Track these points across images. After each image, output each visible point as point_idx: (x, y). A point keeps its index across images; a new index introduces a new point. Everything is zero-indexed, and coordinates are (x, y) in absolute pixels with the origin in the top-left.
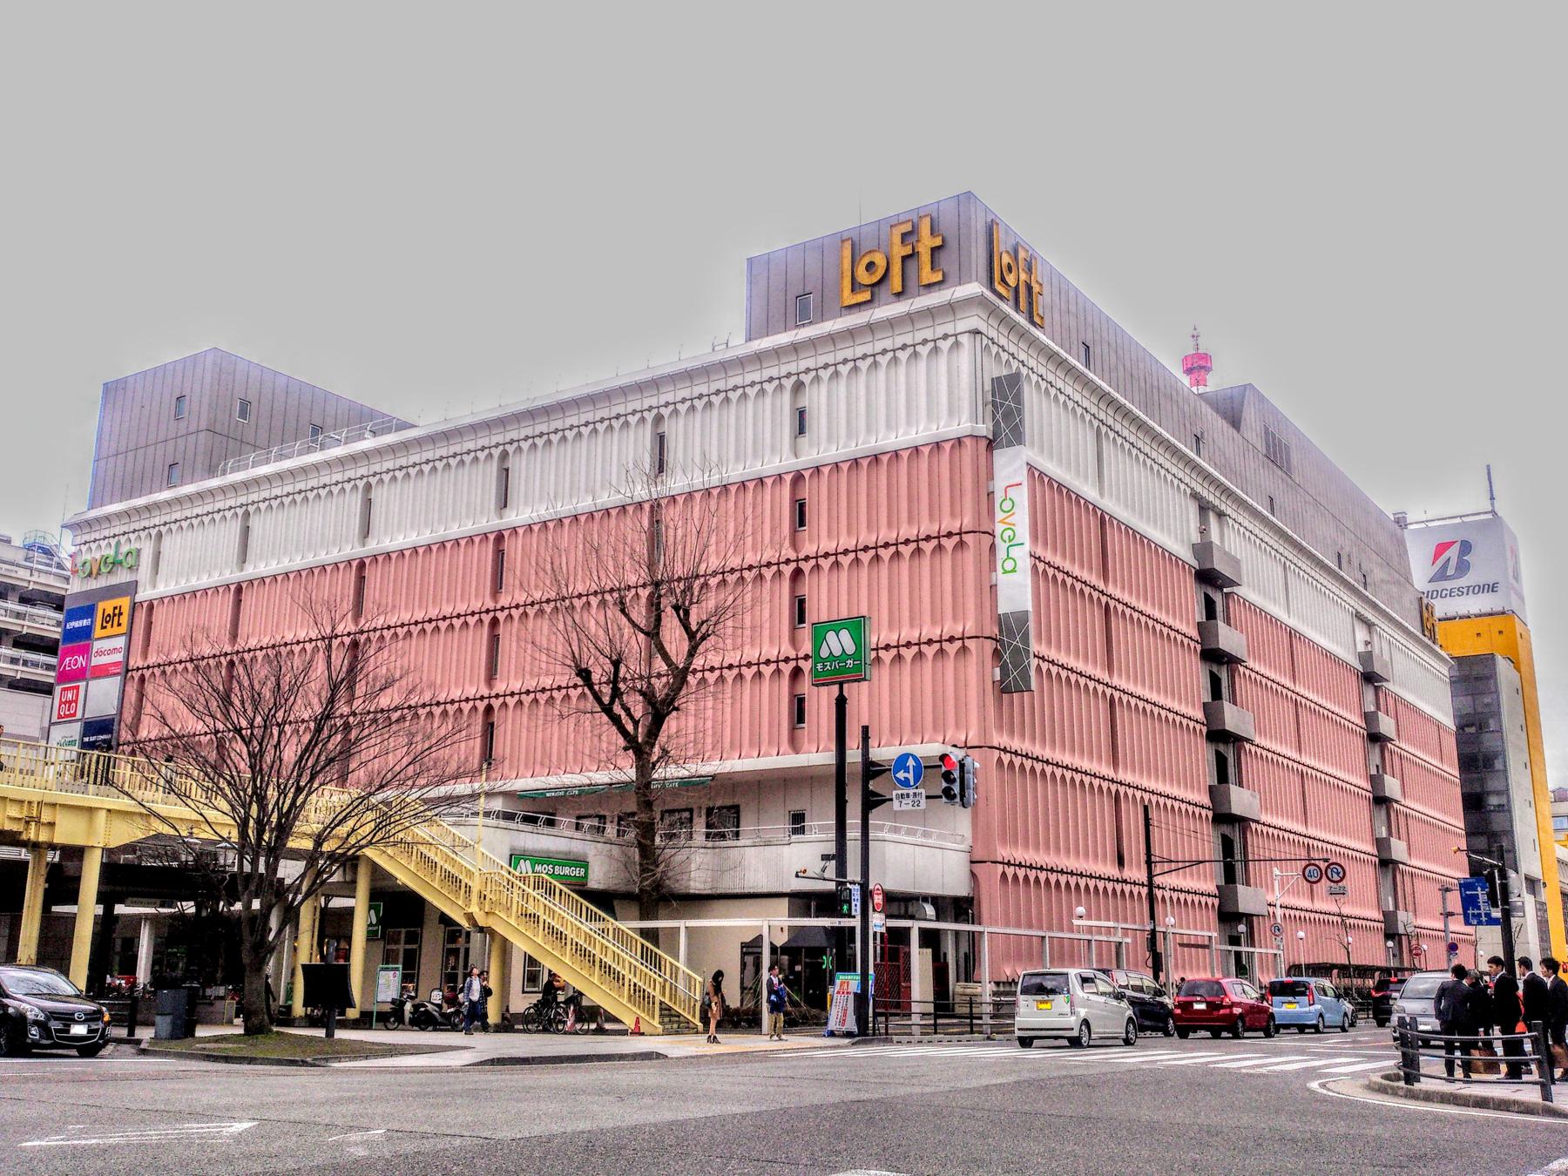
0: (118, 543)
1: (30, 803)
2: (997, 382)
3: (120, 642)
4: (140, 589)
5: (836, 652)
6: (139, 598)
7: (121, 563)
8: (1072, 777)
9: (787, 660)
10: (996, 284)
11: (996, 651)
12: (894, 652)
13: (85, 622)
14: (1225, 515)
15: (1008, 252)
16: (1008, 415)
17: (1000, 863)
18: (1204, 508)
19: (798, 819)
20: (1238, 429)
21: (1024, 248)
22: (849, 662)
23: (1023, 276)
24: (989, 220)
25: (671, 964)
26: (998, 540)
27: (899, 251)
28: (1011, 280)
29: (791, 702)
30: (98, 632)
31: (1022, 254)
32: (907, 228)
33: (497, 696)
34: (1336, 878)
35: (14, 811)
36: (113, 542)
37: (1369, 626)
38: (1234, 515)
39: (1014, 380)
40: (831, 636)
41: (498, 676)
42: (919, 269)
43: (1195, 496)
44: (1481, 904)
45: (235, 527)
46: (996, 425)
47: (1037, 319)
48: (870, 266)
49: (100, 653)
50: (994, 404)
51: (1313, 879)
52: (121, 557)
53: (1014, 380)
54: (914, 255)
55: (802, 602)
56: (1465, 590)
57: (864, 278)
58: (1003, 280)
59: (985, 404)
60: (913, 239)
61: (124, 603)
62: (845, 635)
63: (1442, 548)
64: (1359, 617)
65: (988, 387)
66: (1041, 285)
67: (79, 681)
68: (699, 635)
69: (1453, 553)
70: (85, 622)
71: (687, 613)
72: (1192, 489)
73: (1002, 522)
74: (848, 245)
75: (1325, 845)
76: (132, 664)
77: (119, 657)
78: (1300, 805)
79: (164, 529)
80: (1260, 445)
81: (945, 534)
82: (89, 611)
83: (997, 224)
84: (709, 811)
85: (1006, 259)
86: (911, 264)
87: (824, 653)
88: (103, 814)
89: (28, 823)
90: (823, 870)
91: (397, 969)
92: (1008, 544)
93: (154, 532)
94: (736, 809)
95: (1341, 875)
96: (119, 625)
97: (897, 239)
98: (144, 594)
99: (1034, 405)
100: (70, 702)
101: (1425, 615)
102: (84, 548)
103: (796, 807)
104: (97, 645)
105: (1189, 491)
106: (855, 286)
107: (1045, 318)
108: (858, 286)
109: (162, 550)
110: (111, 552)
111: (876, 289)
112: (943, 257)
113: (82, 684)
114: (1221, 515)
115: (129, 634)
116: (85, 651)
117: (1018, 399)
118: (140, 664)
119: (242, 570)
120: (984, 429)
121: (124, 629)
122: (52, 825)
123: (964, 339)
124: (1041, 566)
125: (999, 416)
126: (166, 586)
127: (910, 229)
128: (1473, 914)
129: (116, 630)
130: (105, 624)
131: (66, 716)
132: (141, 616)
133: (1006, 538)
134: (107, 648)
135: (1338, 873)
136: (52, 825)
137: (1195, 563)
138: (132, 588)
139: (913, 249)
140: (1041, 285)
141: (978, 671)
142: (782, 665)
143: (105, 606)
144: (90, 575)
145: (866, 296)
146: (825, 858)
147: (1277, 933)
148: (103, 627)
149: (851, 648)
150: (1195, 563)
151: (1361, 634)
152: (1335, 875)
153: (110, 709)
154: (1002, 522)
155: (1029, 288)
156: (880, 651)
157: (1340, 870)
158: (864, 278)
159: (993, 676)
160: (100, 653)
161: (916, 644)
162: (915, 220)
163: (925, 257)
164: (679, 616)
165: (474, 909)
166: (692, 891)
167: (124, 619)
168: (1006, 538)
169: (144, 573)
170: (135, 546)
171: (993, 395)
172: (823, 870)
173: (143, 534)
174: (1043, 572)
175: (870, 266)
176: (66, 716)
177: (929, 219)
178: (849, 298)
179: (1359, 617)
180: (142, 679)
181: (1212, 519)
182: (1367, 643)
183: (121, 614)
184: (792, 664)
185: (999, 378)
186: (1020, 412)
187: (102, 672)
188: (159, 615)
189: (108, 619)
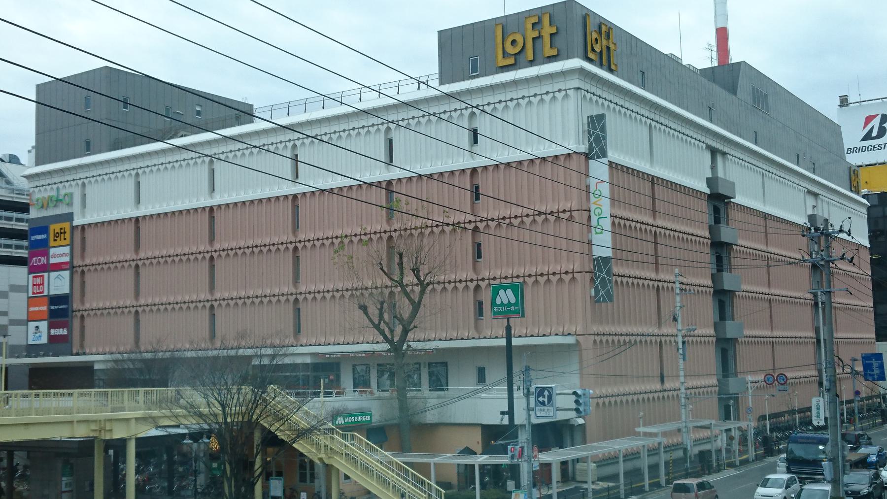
0: (58, 188)
1: (100, 421)
2: (591, 119)
3: (67, 250)
4: (75, 218)
5: (506, 302)
6: (75, 223)
7: (61, 201)
8: (635, 117)
9: (472, 280)
10: (589, 53)
11: (592, 279)
12: (533, 278)
13: (43, 237)
14: (726, 154)
15: (595, 31)
16: (598, 140)
17: (593, 335)
18: (714, 152)
19: (481, 376)
20: (734, 92)
21: (604, 24)
22: (512, 307)
23: (605, 42)
24: (584, 13)
25: (428, 484)
26: (592, 214)
27: (531, 34)
28: (597, 48)
29: (475, 304)
30: (52, 243)
31: (604, 29)
32: (535, 20)
33: (301, 293)
34: (782, 382)
35: (93, 427)
36: (55, 187)
37: (816, 195)
38: (732, 152)
39: (601, 117)
40: (501, 292)
41: (300, 281)
42: (543, 47)
43: (708, 147)
44: (874, 369)
45: (131, 183)
46: (591, 145)
47: (613, 67)
48: (514, 42)
49: (55, 256)
50: (589, 132)
51: (770, 383)
52: (61, 198)
53: (601, 117)
54: (540, 37)
55: (479, 246)
56: (883, 146)
57: (510, 50)
58: (593, 50)
59: (584, 132)
60: (538, 27)
61: (66, 226)
62: (509, 291)
63: (869, 119)
64: (810, 192)
65: (586, 121)
66: (615, 44)
67: (44, 272)
68: (425, 282)
69: (876, 122)
70: (43, 237)
71: (418, 272)
72: (707, 144)
73: (594, 203)
74: (499, 29)
75: (783, 340)
76: (75, 263)
77: (67, 259)
78: (768, 320)
79: (86, 181)
80: (750, 100)
81: (562, 211)
82: (44, 230)
83: (589, 15)
84: (430, 364)
85: (595, 35)
86: (538, 42)
87: (498, 302)
88: (133, 421)
89: (100, 431)
90: (502, 420)
91: (281, 479)
92: (598, 217)
93: (80, 182)
94: (445, 364)
95: (785, 380)
96: (65, 239)
97: (529, 26)
98: (77, 222)
99: (614, 125)
100: (39, 285)
101: (853, 177)
102: (36, 190)
103: (481, 365)
104: (52, 251)
105: (704, 146)
106: (505, 54)
107: (618, 65)
108: (506, 55)
109: (86, 193)
110: (54, 193)
111: (518, 57)
112: (558, 40)
113: (46, 275)
114: (724, 154)
115: (72, 245)
116: (46, 254)
117: (603, 130)
118: (81, 263)
119: (138, 208)
120: (583, 148)
121: (68, 242)
122: (111, 430)
123: (570, 92)
124: (617, 221)
125: (592, 140)
126: (91, 217)
127: (537, 21)
128: (870, 375)
129: (63, 242)
130: (56, 238)
131: (38, 293)
132: (78, 235)
133: (597, 214)
134: (59, 253)
135: (783, 380)
136: (111, 430)
137: (708, 191)
138: (69, 217)
139: (539, 33)
140: (615, 44)
141: (583, 290)
142: (469, 283)
143: (55, 227)
144: (42, 207)
145: (511, 61)
146: (503, 413)
147: (749, 412)
148: (55, 240)
149: (513, 300)
150: (708, 191)
151: (811, 201)
152: (782, 380)
153: (66, 290)
154: (594, 203)
155: (608, 48)
156: (526, 278)
157: (784, 377)
158: (510, 50)
159: (590, 292)
160: (55, 256)
161: (546, 275)
162: (540, 15)
163: (547, 39)
164: (414, 273)
165: (323, 456)
166: (428, 422)
167: (68, 236)
168: (597, 214)
169: (76, 209)
170: (68, 191)
171: (589, 127)
172: (502, 420)
173: (73, 183)
174: (619, 226)
175: (514, 42)
176: (38, 293)
177: (548, 15)
178: (502, 62)
179: (810, 192)
180: (83, 272)
181: (719, 159)
182: (814, 207)
183: (65, 232)
184: (475, 283)
185: (591, 117)
186: (604, 138)
187: (58, 267)
188: (89, 234)
189: (57, 235)
